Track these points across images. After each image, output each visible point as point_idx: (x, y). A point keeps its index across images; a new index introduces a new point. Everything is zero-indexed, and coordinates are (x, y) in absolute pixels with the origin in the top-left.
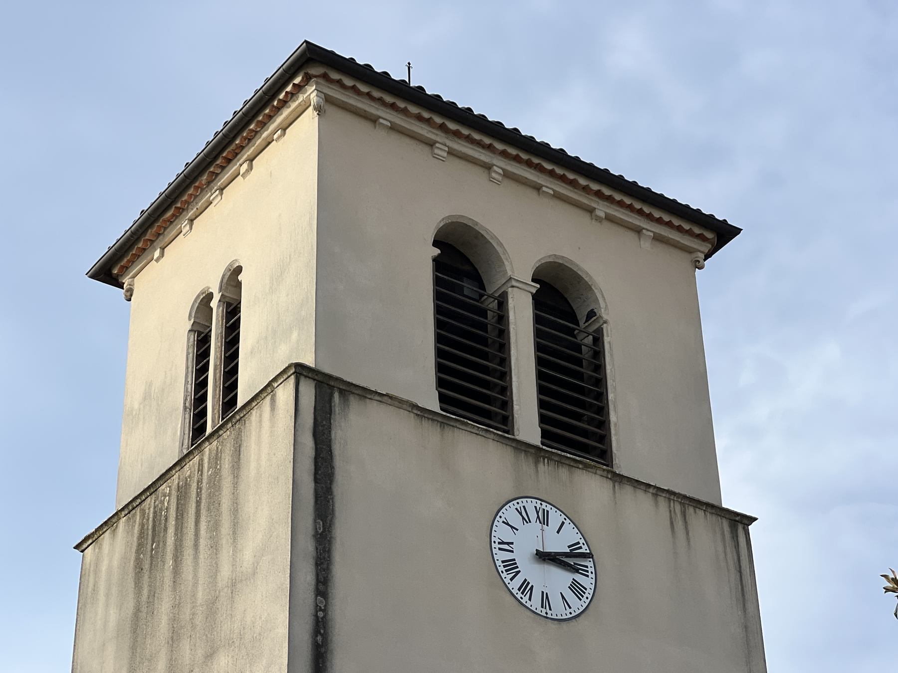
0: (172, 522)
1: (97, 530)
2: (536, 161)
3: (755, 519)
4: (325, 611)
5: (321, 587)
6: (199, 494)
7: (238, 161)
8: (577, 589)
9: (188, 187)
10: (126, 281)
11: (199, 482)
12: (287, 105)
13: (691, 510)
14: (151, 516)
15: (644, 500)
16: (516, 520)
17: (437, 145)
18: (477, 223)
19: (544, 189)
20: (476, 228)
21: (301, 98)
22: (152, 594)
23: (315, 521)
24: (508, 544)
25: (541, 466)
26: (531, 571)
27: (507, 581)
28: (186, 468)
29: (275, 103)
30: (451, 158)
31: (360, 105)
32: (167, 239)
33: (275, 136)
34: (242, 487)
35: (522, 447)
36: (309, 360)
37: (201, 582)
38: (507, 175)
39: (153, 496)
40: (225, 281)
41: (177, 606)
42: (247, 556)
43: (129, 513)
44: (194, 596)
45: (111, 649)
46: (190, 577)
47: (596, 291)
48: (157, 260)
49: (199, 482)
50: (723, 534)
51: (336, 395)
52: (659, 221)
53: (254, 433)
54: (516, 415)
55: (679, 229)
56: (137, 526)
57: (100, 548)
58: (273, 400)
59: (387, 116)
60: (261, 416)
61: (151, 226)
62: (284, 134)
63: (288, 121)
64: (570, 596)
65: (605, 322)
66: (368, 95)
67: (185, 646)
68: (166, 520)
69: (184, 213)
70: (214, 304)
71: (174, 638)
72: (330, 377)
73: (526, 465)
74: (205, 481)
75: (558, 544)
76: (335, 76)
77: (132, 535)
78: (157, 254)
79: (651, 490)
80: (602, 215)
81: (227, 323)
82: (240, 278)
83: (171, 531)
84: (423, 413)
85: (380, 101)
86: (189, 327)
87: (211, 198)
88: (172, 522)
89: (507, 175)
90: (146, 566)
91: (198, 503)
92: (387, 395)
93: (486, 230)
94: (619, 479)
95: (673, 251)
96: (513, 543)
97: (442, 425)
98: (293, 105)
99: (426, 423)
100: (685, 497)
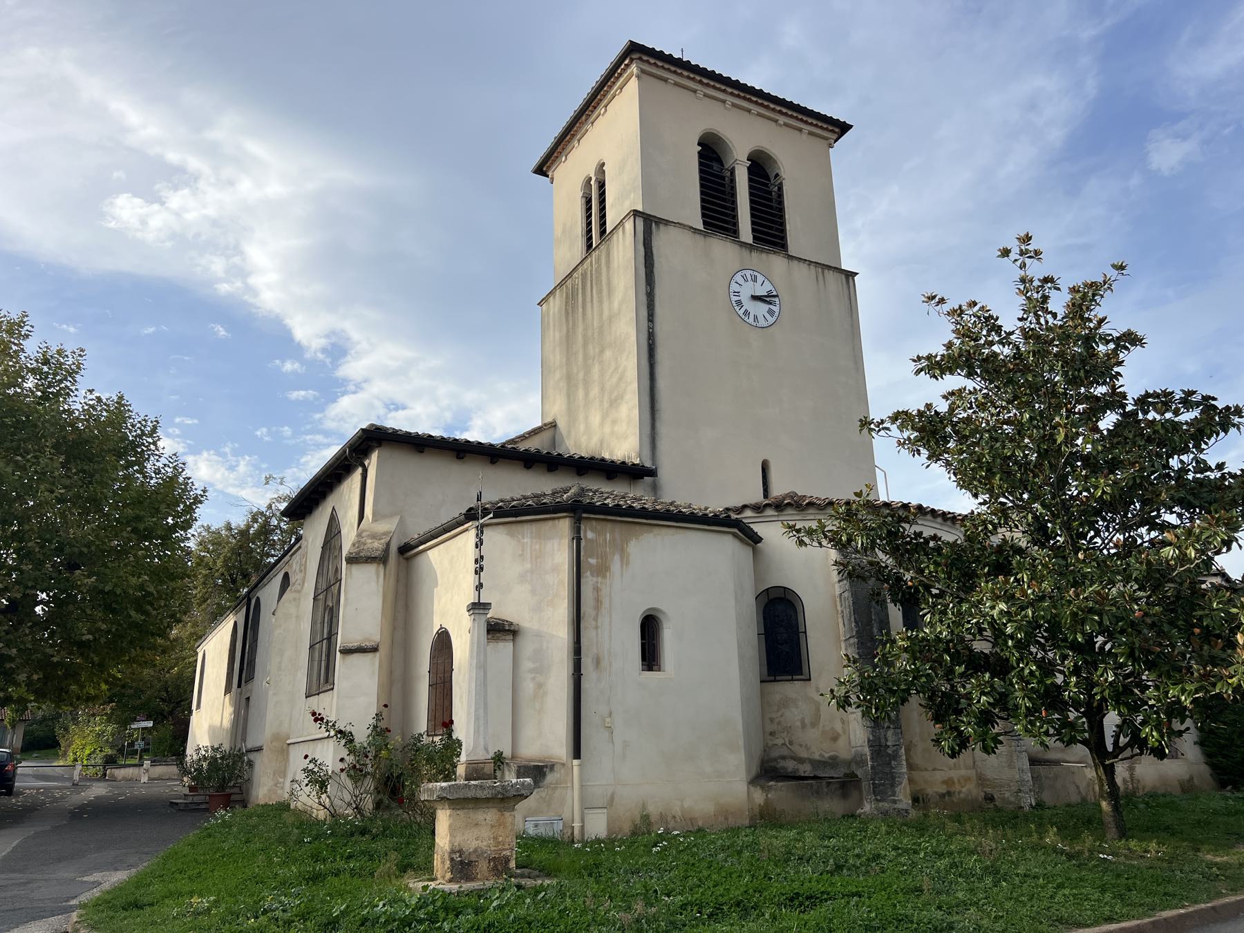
0: (580, 291)
2: (748, 96)
4: (653, 329)
6: (591, 277)
8: (771, 312)
11: (591, 271)
15: (803, 267)
16: (761, 319)
21: (629, 71)
22: (574, 325)
23: (646, 288)
25: (753, 253)
31: (659, 73)
34: (611, 272)
35: (743, 245)
38: (734, 105)
41: (585, 329)
42: (616, 305)
44: (593, 324)
45: (558, 350)
49: (591, 271)
51: (654, 224)
52: (811, 124)
55: (821, 128)
61: (560, 144)
64: (768, 316)
66: (662, 67)
67: (590, 347)
71: (585, 345)
73: (745, 253)
74: (594, 269)
75: (761, 292)
76: (645, 58)
83: (580, 295)
88: (580, 291)
89: (734, 105)
90: (570, 311)
94: (791, 258)
98: (625, 75)
99: (697, 236)
100: (824, 265)
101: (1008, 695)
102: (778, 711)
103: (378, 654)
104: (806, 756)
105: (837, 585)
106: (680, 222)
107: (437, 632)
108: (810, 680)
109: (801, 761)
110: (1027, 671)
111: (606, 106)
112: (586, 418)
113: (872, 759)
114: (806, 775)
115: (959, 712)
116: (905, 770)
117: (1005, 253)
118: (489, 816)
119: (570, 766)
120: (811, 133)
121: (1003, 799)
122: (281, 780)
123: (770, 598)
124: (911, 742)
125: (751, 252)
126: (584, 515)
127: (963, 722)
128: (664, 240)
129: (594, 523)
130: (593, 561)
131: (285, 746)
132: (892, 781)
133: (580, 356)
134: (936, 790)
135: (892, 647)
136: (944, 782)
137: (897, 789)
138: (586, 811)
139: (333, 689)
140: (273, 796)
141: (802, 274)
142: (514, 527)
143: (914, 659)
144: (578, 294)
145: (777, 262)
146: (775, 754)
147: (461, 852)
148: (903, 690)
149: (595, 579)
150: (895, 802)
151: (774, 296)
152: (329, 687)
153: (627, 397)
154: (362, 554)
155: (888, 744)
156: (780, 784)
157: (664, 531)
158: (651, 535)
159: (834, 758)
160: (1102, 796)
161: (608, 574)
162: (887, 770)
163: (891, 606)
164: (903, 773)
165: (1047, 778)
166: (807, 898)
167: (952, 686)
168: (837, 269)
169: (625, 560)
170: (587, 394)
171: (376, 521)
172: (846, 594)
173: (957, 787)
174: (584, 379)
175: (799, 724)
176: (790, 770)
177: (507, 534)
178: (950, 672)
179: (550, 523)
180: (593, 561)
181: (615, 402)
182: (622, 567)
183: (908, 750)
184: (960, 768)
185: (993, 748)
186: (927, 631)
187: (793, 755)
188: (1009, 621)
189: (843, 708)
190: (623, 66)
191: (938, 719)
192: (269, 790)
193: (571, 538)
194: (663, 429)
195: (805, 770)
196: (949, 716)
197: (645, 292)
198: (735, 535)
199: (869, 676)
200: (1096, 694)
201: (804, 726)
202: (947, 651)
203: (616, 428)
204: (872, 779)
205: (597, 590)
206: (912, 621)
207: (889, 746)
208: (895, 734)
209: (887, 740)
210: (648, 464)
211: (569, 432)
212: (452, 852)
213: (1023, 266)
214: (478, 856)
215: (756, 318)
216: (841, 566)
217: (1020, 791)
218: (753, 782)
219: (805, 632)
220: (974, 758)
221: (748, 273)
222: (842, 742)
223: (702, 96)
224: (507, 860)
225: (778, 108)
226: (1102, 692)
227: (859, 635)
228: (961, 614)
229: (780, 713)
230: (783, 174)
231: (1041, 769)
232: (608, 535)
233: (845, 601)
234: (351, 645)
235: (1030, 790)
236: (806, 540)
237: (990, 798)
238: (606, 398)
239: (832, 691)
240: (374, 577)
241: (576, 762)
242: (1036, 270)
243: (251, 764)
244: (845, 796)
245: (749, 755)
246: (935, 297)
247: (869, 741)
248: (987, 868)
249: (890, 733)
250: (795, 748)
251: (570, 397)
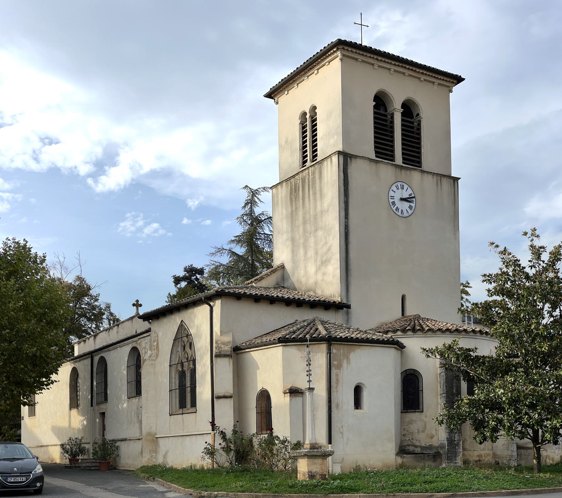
0: (301, 189)
1: (276, 185)
2: (404, 65)
3: (461, 178)
4: (347, 223)
5: (346, 216)
6: (309, 182)
8: (410, 207)
9: (298, 75)
10: (276, 99)
11: (309, 179)
13: (443, 178)
14: (294, 185)
15: (430, 177)
16: (405, 212)
17: (375, 65)
18: (386, 90)
19: (406, 74)
20: (386, 92)
21: (335, 54)
22: (296, 208)
23: (344, 198)
24: (393, 197)
25: (402, 171)
26: (399, 204)
27: (392, 208)
28: (304, 173)
30: (379, 68)
31: (353, 56)
33: (326, 64)
34: (322, 184)
35: (397, 166)
36: (341, 150)
37: (311, 208)
38: (395, 71)
39: (294, 179)
40: (311, 109)
41: (304, 214)
42: (325, 205)
44: (310, 212)
45: (285, 221)
46: (308, 206)
47: (420, 107)
48: (286, 95)
49: (309, 179)
50: (451, 184)
51: (349, 158)
52: (440, 79)
53: (325, 169)
54: (395, 155)
55: (446, 81)
56: (289, 187)
57: (278, 190)
58: (331, 159)
59: (360, 58)
60: (327, 164)
61: (285, 84)
62: (329, 64)
64: (409, 210)
65: (422, 118)
66: (356, 52)
67: (308, 226)
68: (299, 187)
70: (308, 116)
71: (305, 223)
72: (347, 154)
73: (398, 171)
74: (310, 179)
75: (406, 195)
76: (346, 48)
77: (288, 188)
78: (286, 92)
79: (432, 174)
80: (422, 79)
81: (312, 124)
82: (316, 111)
83: (301, 191)
84: (371, 160)
85: (359, 54)
86: (299, 123)
88: (301, 189)
89: (395, 71)
90: (294, 199)
91: (309, 185)
92: (362, 157)
93: (388, 92)
94: (423, 172)
95: (444, 87)
97: (376, 163)
98: (333, 56)
99: (372, 163)
100: (441, 175)
101: (502, 421)
102: (407, 425)
103: (232, 399)
104: (419, 445)
105: (439, 369)
106: (363, 155)
107: (261, 390)
108: (423, 412)
109: (416, 446)
110: (510, 413)
111: (318, 69)
112: (305, 267)
113: (448, 446)
114: (418, 452)
115: (484, 427)
116: (461, 450)
117: (526, 234)
118: (319, 461)
119: (327, 447)
120: (439, 84)
121: (503, 463)
122: (154, 455)
123: (407, 373)
124: (465, 439)
125: (401, 170)
126: (332, 342)
127: (486, 431)
128: (355, 167)
129: (336, 345)
130: (336, 363)
131: (155, 439)
132: (455, 454)
133: (301, 229)
134: (474, 459)
135: (462, 402)
136: (478, 456)
137: (457, 458)
138: (333, 464)
139: (196, 412)
140: (151, 462)
141: (429, 180)
142: (300, 347)
143: (470, 407)
144: (299, 190)
145: (416, 175)
146: (405, 444)
147: (311, 472)
148: (464, 419)
149: (336, 371)
150: (456, 463)
151: (412, 198)
152: (194, 411)
153: (333, 261)
154: (222, 353)
155: (455, 439)
156: (408, 456)
157: (365, 347)
158: (360, 350)
159: (431, 445)
160: (534, 458)
161: (341, 368)
162: (454, 450)
163: (462, 382)
164: (460, 452)
165: (524, 455)
166: (429, 482)
167: (484, 417)
168: (449, 176)
169: (349, 362)
170: (306, 253)
171: (222, 335)
172: (443, 374)
173: (483, 458)
174: (304, 244)
175: (416, 431)
176: (411, 450)
177: (297, 350)
178: (483, 411)
179: (317, 345)
180: (336, 363)
181: (325, 262)
182: (347, 364)
183: (463, 442)
184: (486, 450)
185: (495, 441)
186: (476, 396)
187: (412, 444)
188: (504, 396)
189: (441, 424)
190: (332, 51)
191: (476, 429)
192: (148, 460)
193: (327, 353)
194: (353, 281)
195: (418, 450)
196: (481, 428)
197: (343, 201)
198: (395, 348)
199: (452, 413)
200: (531, 422)
201: (419, 432)
202: (482, 404)
203: (325, 278)
204: (447, 454)
205: (337, 375)
206: (471, 392)
207: (455, 441)
208: (459, 435)
209: (455, 438)
210: (345, 301)
211: (293, 273)
212: (309, 472)
213: (532, 240)
214: (316, 474)
215: (402, 211)
216: (443, 365)
217: (510, 460)
218: (397, 454)
219: (422, 390)
220: (492, 446)
221: (399, 184)
222: (435, 439)
223: (377, 67)
224: (325, 476)
225: (421, 71)
226: (532, 421)
227: (447, 393)
228: (489, 391)
229: (408, 426)
230: (422, 115)
231: (522, 451)
232: (342, 350)
233: (442, 376)
234: (220, 395)
235: (515, 460)
236: (430, 355)
237: (498, 463)
238: (319, 259)
239: (437, 418)
240: (228, 364)
241: (330, 445)
242: (538, 243)
243: (118, 448)
244: (434, 461)
245: (396, 443)
246: (494, 243)
247: (447, 438)
248: (485, 477)
249: (456, 435)
250: (414, 441)
251: (294, 252)
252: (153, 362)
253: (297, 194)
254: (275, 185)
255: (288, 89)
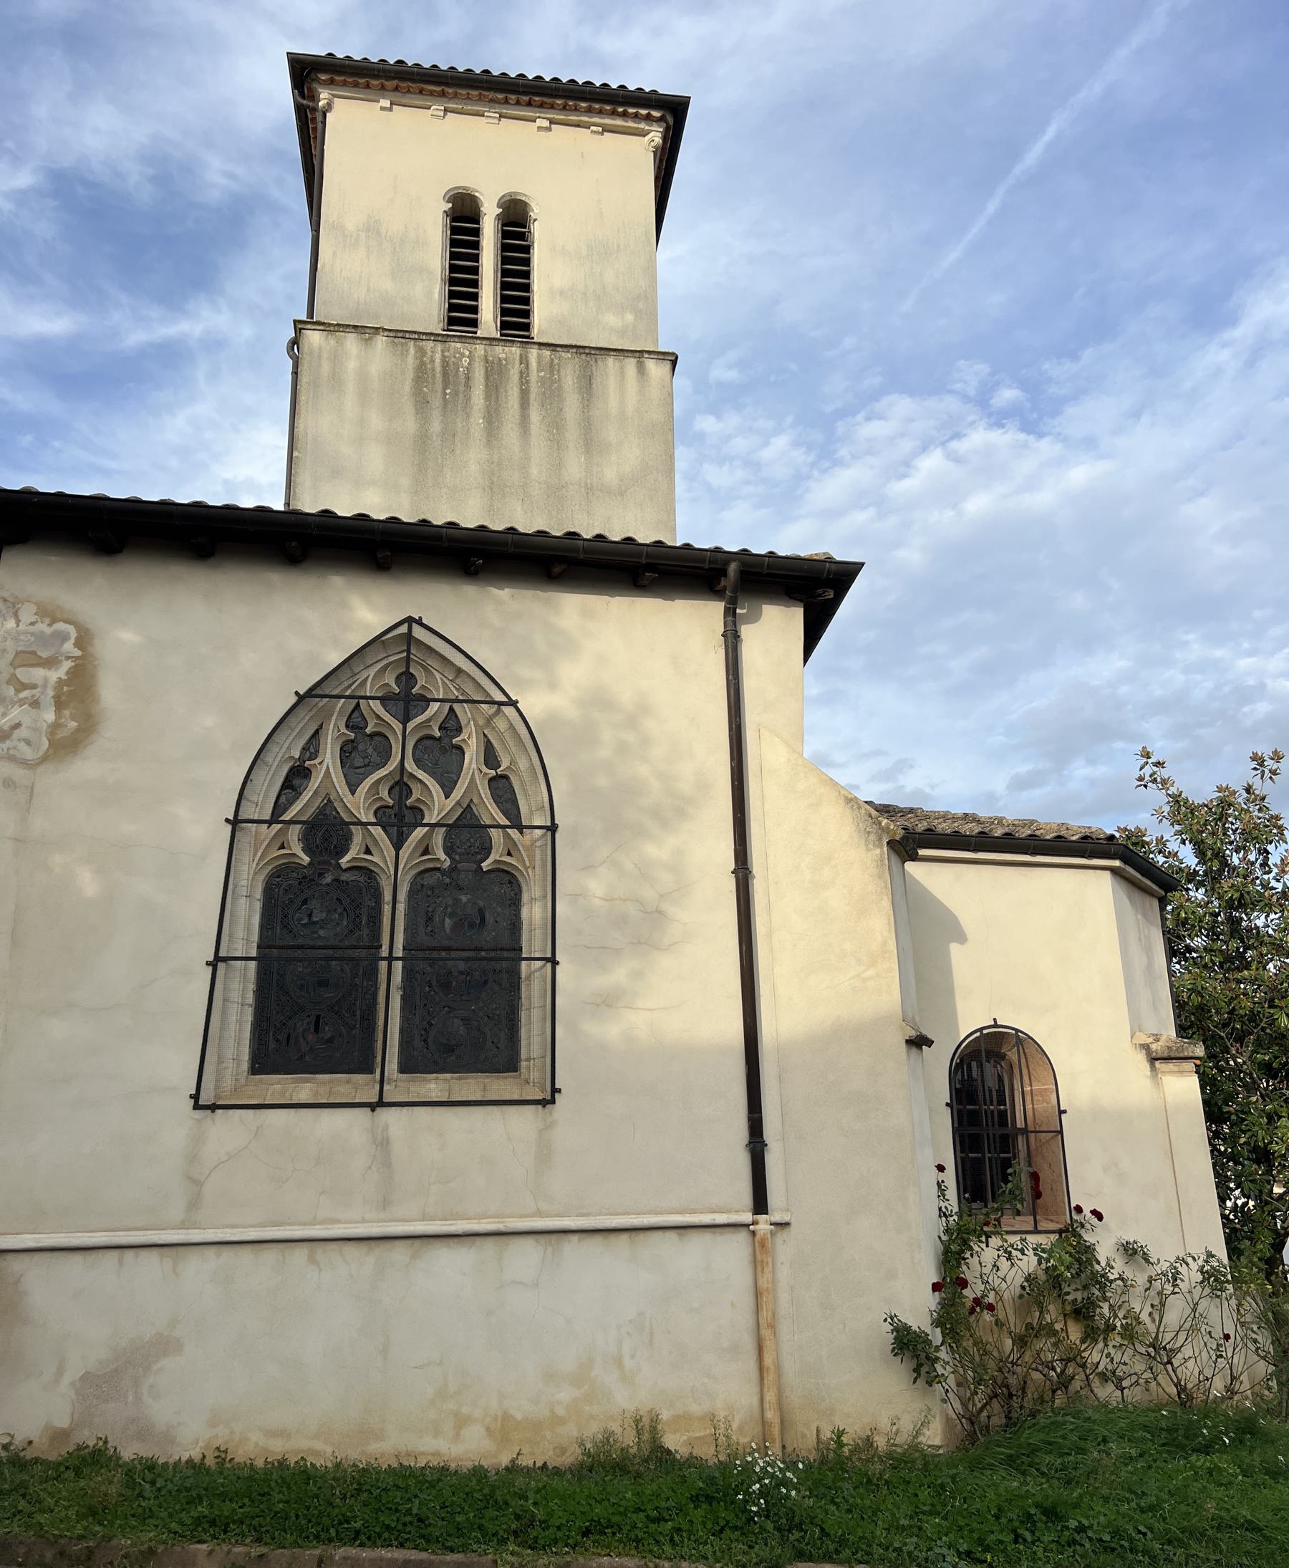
7: (540, 112)
12: (626, 119)
29: (621, 110)
32: (404, 101)
43: (395, 337)
62: (602, 134)
63: (613, 129)
69: (445, 99)
87: (486, 114)
96: (945, 1169)
98: (631, 124)
107: (981, 1030)
190: (644, 112)
252: (19, 773)
253: (456, 393)
254: (330, 325)
255: (397, 97)
